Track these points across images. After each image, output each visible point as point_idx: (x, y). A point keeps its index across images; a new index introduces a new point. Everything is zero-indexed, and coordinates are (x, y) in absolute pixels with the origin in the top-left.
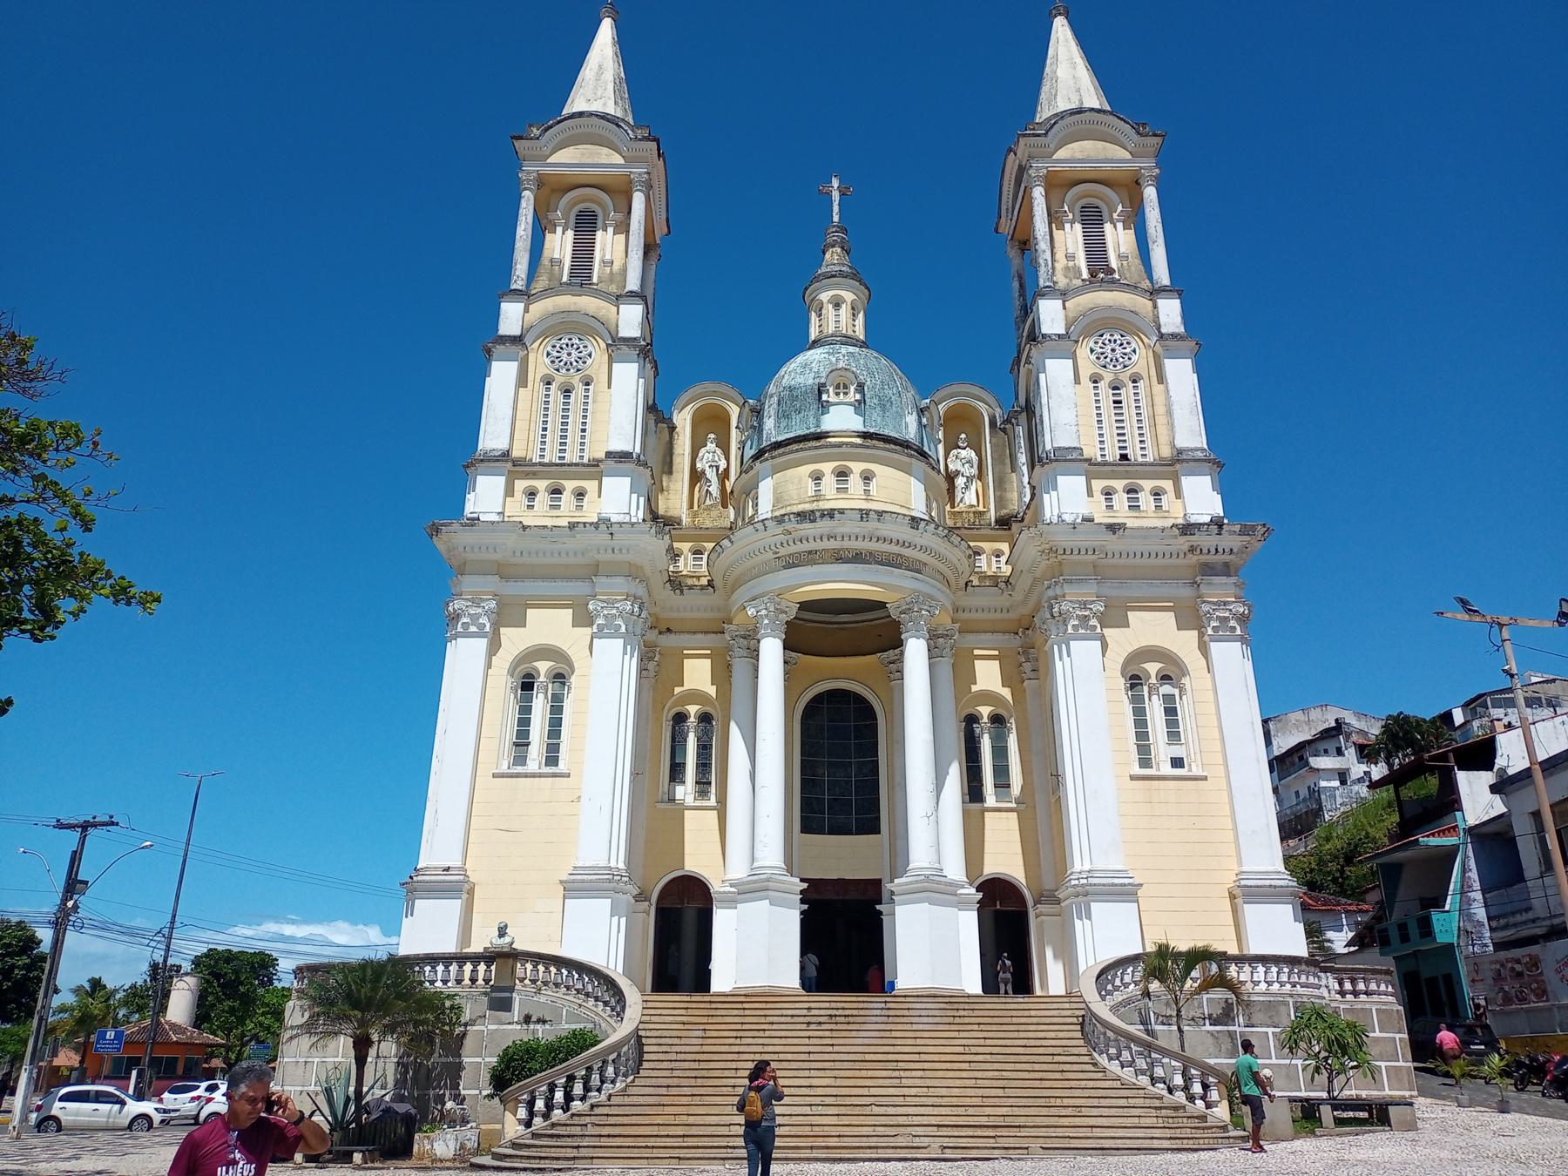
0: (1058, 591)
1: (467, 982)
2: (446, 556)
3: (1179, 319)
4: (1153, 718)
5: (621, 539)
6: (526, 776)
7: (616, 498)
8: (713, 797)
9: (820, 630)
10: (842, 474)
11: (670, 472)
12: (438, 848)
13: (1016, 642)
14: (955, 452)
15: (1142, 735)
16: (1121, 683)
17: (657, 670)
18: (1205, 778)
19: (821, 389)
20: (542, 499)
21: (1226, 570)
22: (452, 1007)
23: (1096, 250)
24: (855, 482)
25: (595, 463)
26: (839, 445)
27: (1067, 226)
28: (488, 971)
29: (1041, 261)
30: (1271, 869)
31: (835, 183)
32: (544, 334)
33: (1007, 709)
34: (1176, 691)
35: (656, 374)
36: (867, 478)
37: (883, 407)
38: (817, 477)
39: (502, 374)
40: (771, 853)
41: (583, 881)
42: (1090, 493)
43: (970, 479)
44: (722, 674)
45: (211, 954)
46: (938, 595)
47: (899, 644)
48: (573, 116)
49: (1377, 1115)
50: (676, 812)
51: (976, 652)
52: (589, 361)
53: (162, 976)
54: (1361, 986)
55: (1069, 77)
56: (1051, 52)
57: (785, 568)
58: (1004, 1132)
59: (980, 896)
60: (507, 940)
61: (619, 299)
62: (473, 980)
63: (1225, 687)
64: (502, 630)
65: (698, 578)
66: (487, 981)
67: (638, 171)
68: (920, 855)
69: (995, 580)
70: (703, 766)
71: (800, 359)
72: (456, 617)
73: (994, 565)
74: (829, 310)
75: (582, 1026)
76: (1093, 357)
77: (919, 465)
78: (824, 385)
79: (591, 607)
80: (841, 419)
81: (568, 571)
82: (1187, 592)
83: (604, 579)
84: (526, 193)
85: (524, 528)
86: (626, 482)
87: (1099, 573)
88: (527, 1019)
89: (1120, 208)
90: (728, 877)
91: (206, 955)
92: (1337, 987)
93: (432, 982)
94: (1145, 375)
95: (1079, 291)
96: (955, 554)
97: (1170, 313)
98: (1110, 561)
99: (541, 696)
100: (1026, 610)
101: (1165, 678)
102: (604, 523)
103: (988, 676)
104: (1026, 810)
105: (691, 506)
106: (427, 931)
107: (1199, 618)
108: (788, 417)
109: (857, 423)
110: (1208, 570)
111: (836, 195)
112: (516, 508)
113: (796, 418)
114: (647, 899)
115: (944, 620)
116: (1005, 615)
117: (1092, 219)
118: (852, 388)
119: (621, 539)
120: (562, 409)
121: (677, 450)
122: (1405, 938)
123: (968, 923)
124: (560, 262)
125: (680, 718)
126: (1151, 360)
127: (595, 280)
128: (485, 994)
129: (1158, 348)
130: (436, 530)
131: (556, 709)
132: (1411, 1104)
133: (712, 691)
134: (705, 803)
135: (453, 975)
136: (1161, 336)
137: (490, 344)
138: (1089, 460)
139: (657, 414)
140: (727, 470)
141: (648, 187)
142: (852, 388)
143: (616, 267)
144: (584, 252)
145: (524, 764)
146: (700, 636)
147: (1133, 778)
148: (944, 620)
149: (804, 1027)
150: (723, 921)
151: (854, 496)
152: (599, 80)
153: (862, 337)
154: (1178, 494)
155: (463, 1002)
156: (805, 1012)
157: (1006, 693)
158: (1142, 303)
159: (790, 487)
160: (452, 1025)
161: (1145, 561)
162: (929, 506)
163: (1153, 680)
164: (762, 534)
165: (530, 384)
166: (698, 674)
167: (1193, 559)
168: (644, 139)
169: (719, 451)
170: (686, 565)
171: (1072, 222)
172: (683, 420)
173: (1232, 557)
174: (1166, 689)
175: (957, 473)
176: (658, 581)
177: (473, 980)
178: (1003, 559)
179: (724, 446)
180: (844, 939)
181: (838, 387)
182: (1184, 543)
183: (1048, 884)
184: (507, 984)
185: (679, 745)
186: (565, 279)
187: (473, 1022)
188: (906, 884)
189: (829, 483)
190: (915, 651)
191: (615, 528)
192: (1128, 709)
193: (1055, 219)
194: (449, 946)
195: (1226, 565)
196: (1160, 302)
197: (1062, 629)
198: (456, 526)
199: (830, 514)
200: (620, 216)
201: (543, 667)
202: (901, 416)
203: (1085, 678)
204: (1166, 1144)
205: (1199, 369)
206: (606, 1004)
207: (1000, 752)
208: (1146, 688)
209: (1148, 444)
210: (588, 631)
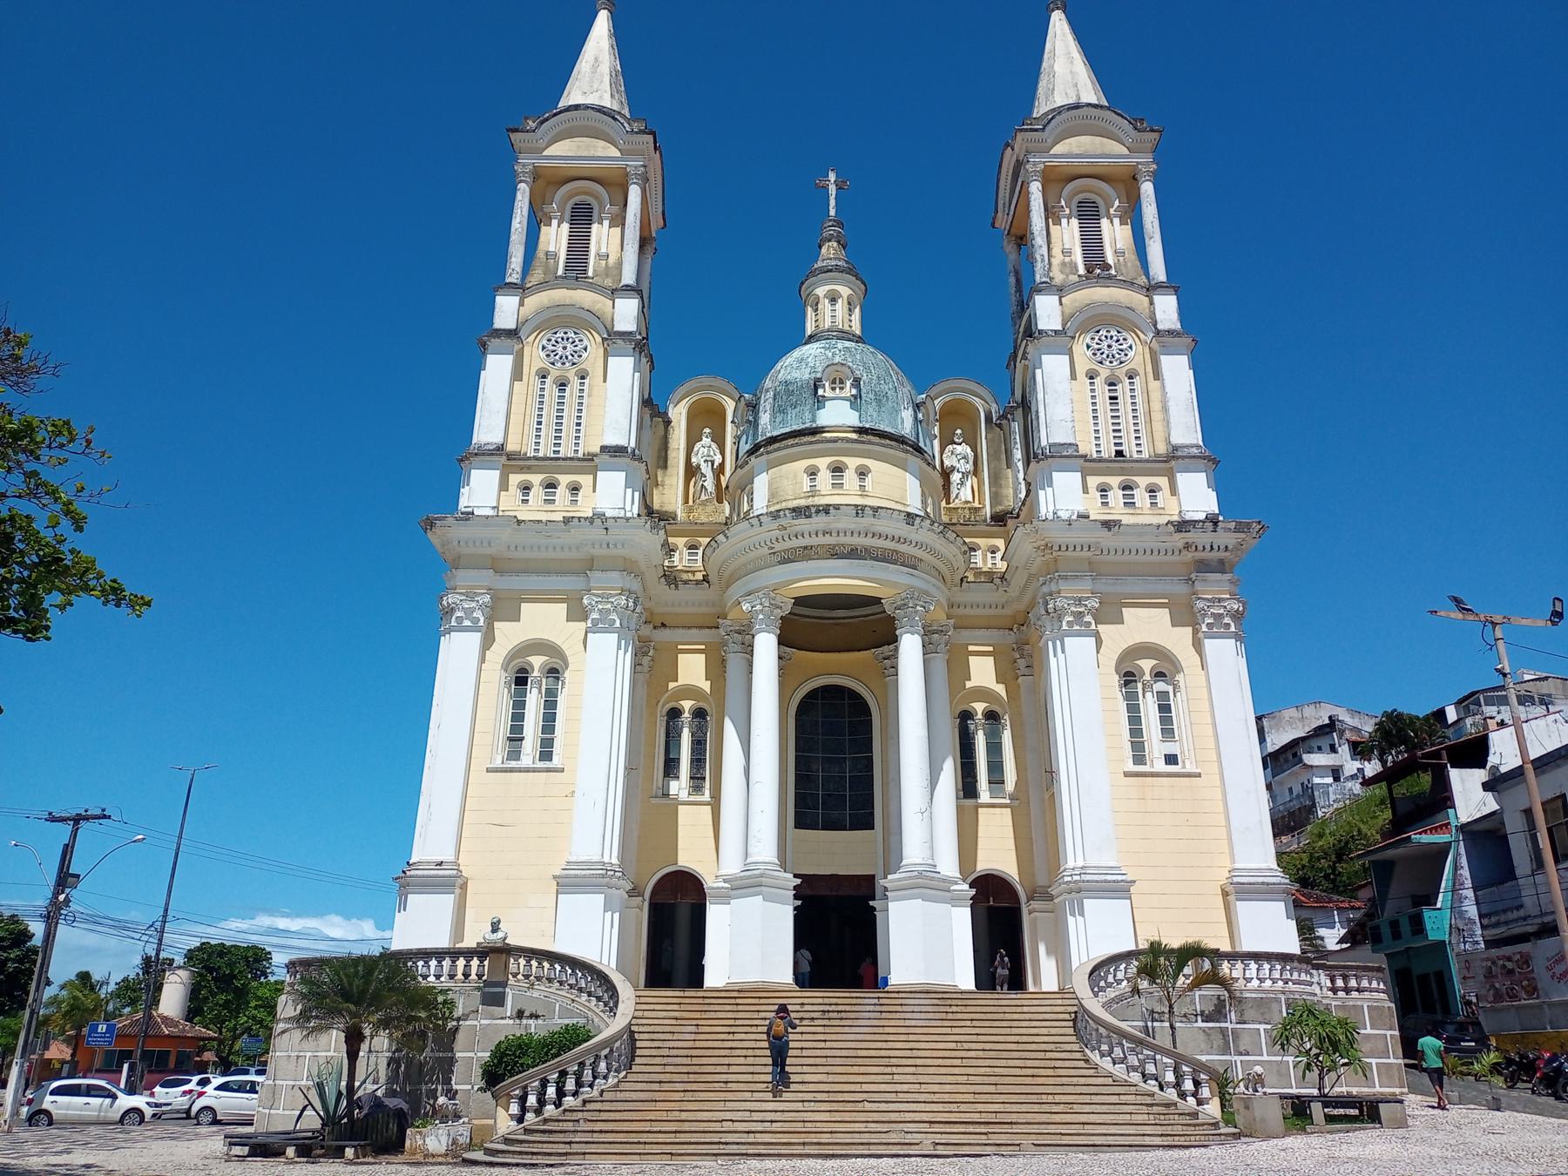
0: (1053, 587)
2: (440, 550)
3: (1175, 316)
4: (1147, 715)
5: (616, 533)
6: (520, 770)
7: (611, 493)
8: (707, 793)
10: (838, 470)
11: (665, 467)
12: (431, 842)
13: (1010, 638)
14: (950, 447)
15: (1136, 731)
16: (1115, 680)
17: (651, 666)
18: (1199, 775)
19: (817, 384)
20: (537, 494)
21: (1221, 567)
22: (445, 1002)
23: (1093, 246)
24: (850, 477)
25: (590, 458)
26: (835, 440)
27: (1064, 221)
28: (481, 965)
30: (1263, 866)
31: (832, 177)
32: (540, 328)
34: (1170, 689)
35: (652, 368)
36: (862, 474)
37: (879, 401)
38: (813, 473)
39: (497, 368)
41: (576, 876)
42: (1085, 490)
43: (965, 475)
44: (717, 669)
45: (204, 947)
46: (933, 591)
47: (894, 640)
49: (1367, 1112)
51: (971, 648)
52: (585, 355)
53: (154, 969)
54: (1353, 983)
55: (1066, 73)
56: (1048, 46)
57: (780, 563)
58: (996, 1129)
59: (973, 892)
60: (500, 935)
61: (614, 292)
62: (466, 975)
63: (1219, 686)
64: (496, 624)
65: (693, 573)
66: (480, 976)
67: (634, 164)
68: (914, 850)
69: (990, 576)
70: (698, 761)
73: (990, 561)
74: (825, 305)
76: (1089, 353)
77: (914, 461)
78: (820, 380)
79: (585, 601)
80: (837, 414)
82: (1182, 589)
83: (598, 574)
84: (522, 186)
85: (519, 522)
86: (620, 477)
88: (520, 1014)
89: (1117, 203)
90: (723, 872)
91: (199, 949)
92: (1329, 984)
93: (425, 977)
94: (1141, 372)
97: (1167, 309)
98: (1105, 558)
99: (535, 691)
100: (1021, 606)
101: (1159, 675)
102: (598, 518)
103: (982, 672)
104: (1019, 806)
106: (420, 925)
107: (1193, 614)
108: (783, 412)
109: (852, 418)
110: (1203, 567)
111: (832, 189)
112: (511, 503)
113: (792, 413)
115: (939, 615)
116: (999, 611)
117: (1089, 214)
118: (848, 383)
119: (616, 533)
120: (557, 405)
121: (673, 444)
122: (1397, 935)
123: (961, 921)
124: (555, 256)
125: (675, 713)
126: (1148, 356)
127: (590, 274)
128: (478, 988)
129: (1155, 345)
130: (430, 524)
131: (550, 704)
132: (1401, 1102)
133: (706, 686)
135: (446, 970)
136: (1158, 333)
137: (485, 338)
139: (652, 408)
140: (722, 465)
141: (644, 180)
142: (848, 383)
143: (612, 260)
144: (579, 245)
146: (694, 631)
147: (1127, 774)
148: (939, 615)
150: (716, 915)
151: (849, 492)
152: (595, 73)
153: (858, 332)
154: (1174, 491)
157: (1000, 689)
158: (1138, 300)
160: (445, 1019)
162: (924, 502)
163: (1147, 677)
164: (757, 529)
165: (525, 377)
166: (692, 669)
167: (1189, 556)
169: (714, 446)
170: (681, 560)
172: (679, 413)
174: (1160, 686)
175: (953, 469)
176: (653, 576)
177: (466, 975)
178: (999, 555)
179: (720, 441)
180: (838, 934)
181: (834, 382)
182: (1179, 540)
183: (1041, 880)
185: (675, 741)
186: (560, 273)
187: (465, 1017)
189: (825, 479)
190: (910, 647)
192: (1122, 706)
193: (1051, 214)
194: (443, 942)
195: (1221, 562)
198: (450, 520)
199: (826, 509)
200: (615, 209)
201: (537, 661)
202: (898, 411)
203: (1079, 674)
204: (1158, 1141)
205: (1194, 366)
206: (599, 999)
207: (994, 749)
208: (1140, 685)
209: (1143, 441)
210: (582, 625)
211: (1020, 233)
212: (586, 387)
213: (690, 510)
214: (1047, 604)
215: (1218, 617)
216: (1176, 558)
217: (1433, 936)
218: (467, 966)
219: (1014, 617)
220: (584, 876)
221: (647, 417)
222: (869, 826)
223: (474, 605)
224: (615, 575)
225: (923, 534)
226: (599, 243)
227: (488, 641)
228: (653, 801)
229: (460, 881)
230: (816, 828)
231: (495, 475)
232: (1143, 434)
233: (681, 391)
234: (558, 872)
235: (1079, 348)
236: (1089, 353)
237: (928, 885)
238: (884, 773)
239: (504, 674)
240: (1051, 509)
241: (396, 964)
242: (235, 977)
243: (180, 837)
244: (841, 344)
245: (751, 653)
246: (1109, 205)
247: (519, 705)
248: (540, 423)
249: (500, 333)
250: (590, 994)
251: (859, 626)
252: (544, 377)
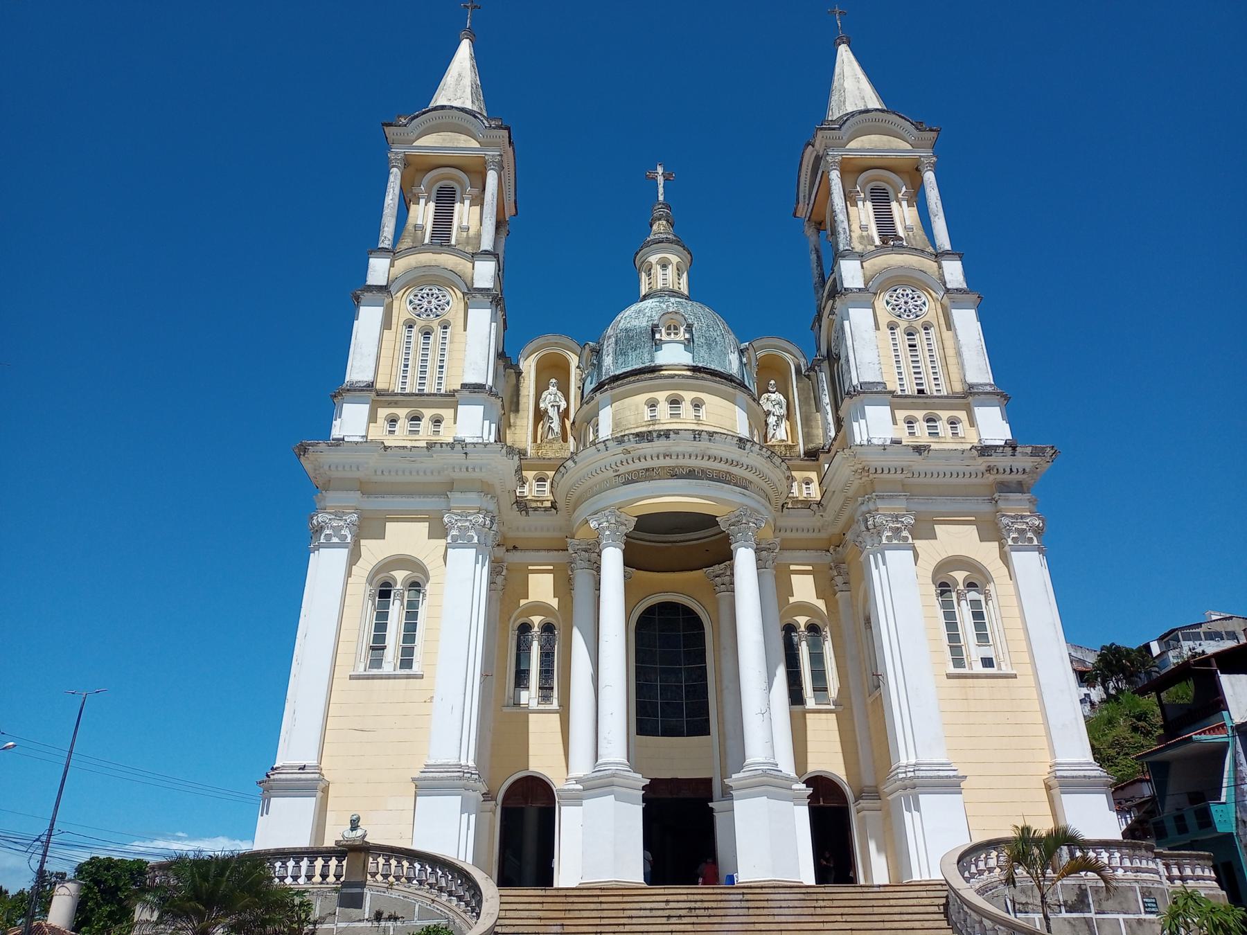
0: (871, 506)
1: (317, 879)
2: (311, 474)
3: (961, 278)
4: (963, 621)
5: (474, 458)
6: (381, 677)
7: (471, 423)
8: (555, 702)
10: (675, 402)
11: (517, 411)
12: (295, 747)
13: (827, 558)
14: (766, 395)
15: (954, 637)
16: (932, 590)
17: (505, 585)
18: (1015, 676)
19: (654, 330)
20: (403, 425)
21: (1020, 488)
22: (302, 904)
23: (885, 221)
24: (686, 410)
25: (452, 394)
26: (672, 377)
27: (860, 203)
28: (339, 866)
29: (841, 230)
30: (1083, 760)
31: (660, 170)
32: (408, 285)
33: (822, 619)
34: (982, 598)
35: (505, 328)
36: (697, 406)
37: (709, 346)
38: (653, 405)
39: (368, 318)
41: (434, 779)
42: (895, 422)
43: (780, 418)
44: (564, 587)
45: (94, 861)
46: (762, 510)
47: (729, 556)
48: (436, 109)
50: (521, 716)
51: (792, 567)
52: (447, 308)
53: (44, 885)
54: (1188, 872)
55: (852, 86)
56: (837, 70)
57: (624, 484)
59: (810, 791)
60: (359, 833)
62: (324, 876)
63: (1026, 589)
64: (363, 542)
65: (542, 501)
66: (338, 877)
67: (492, 154)
69: (807, 504)
70: (546, 673)
71: (634, 307)
72: (319, 529)
73: (805, 492)
74: (657, 270)
75: (435, 922)
76: (889, 308)
77: (741, 395)
78: (657, 326)
79: (446, 520)
80: (673, 354)
81: (429, 489)
82: (987, 508)
83: (458, 495)
84: (394, 170)
85: (386, 448)
86: (479, 409)
87: (907, 490)
88: (378, 916)
89: (904, 189)
90: (571, 775)
91: (88, 863)
93: (282, 879)
94: (935, 324)
96: (776, 474)
97: (954, 272)
98: (916, 480)
99: (397, 603)
100: (837, 530)
101: (971, 585)
102: (460, 442)
103: (804, 589)
104: (843, 711)
105: (535, 441)
106: (283, 826)
107: (999, 530)
108: (625, 354)
109: (687, 359)
110: (1004, 487)
111: (661, 180)
112: (379, 432)
113: (632, 355)
114: (494, 799)
115: (768, 535)
116: (815, 535)
117: (881, 199)
118: (682, 329)
119: (474, 458)
120: (422, 348)
121: (523, 392)
123: (801, 817)
124: (423, 228)
125: (525, 628)
126: (940, 311)
127: (453, 242)
128: (336, 890)
129: (946, 301)
130: (304, 449)
131: (412, 615)
133: (554, 603)
134: (548, 707)
135: (303, 872)
136: (948, 291)
137: (358, 290)
138: (892, 392)
139: (506, 360)
140: (567, 410)
141: (500, 168)
142: (682, 329)
143: (472, 232)
144: (443, 221)
145: (380, 666)
146: (543, 553)
147: (949, 676)
148: (768, 535)
149: (664, 920)
152: (459, 81)
153: (686, 293)
154: (972, 422)
155: (312, 898)
156: (663, 905)
157: (821, 604)
158: (929, 265)
159: (628, 413)
160: (301, 922)
161: (947, 479)
162: (751, 432)
163: (961, 587)
164: (604, 454)
165: (394, 327)
166: (541, 588)
167: (991, 478)
168: (500, 127)
169: (559, 394)
170: (530, 491)
171: (864, 201)
172: (528, 366)
173: (1025, 476)
174: (973, 595)
176: (507, 501)
177: (324, 876)
179: (564, 389)
180: (682, 835)
181: (669, 328)
182: (982, 463)
183: (868, 781)
184: (359, 879)
185: (524, 653)
186: (427, 241)
187: (322, 920)
188: (745, 778)
189: (663, 410)
191: (469, 448)
192: (940, 613)
193: (850, 198)
195: (1020, 483)
196: (945, 264)
197: (876, 541)
198: (322, 446)
199: (666, 434)
201: (400, 576)
202: (726, 354)
203: (899, 585)
205: (981, 318)
206: (460, 898)
207: (817, 659)
208: (954, 595)
209: (942, 381)
210: (442, 542)
211: (819, 219)
212: (448, 336)
213: (539, 447)
214: (866, 521)
215: (1022, 532)
216: (979, 480)
217: (1221, 829)
218: (326, 867)
219: (829, 540)
220: (442, 779)
221: (501, 368)
223: (342, 523)
224: (473, 495)
225: (753, 458)
226: (461, 218)
227: (354, 557)
228: (506, 710)
229: (321, 785)
230: (680, 734)
231: (364, 409)
232: (940, 376)
233: (530, 347)
234: (417, 775)
235: (880, 303)
236: (889, 308)
237: (769, 783)
238: (719, 681)
239: (369, 588)
240: (865, 438)
241: (254, 867)
242: (119, 889)
243: (71, 752)
244: (672, 300)
245: (598, 569)
246: (897, 191)
247: (382, 616)
248: (406, 366)
249: (371, 288)
250: (450, 894)
252: (411, 327)
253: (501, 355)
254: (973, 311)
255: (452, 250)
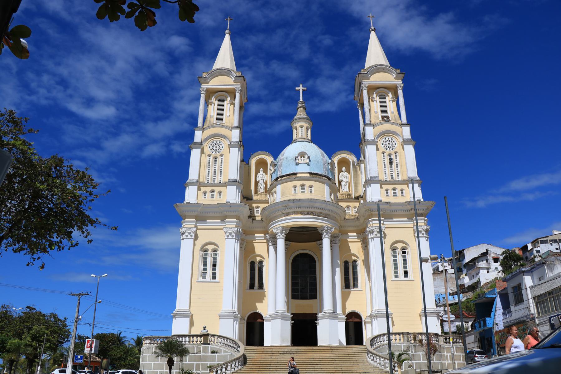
9: (295, 235)
20: (208, 194)
38: (295, 187)
39: (195, 154)
40: (282, 307)
61: (232, 129)
68: (327, 305)
95: (380, 124)
97: (406, 132)
112: (202, 201)
120: (215, 162)
123: (342, 326)
150: (267, 325)
151: (306, 195)
175: (342, 180)
179: (266, 172)
180: (304, 331)
190: (326, 242)
194: (187, 332)
201: (399, 246)
222: (316, 298)
230: (298, 299)
231: (196, 188)
249: (195, 143)
251: (312, 235)
253: (242, 161)
254: (411, 146)
255: (224, 127)
